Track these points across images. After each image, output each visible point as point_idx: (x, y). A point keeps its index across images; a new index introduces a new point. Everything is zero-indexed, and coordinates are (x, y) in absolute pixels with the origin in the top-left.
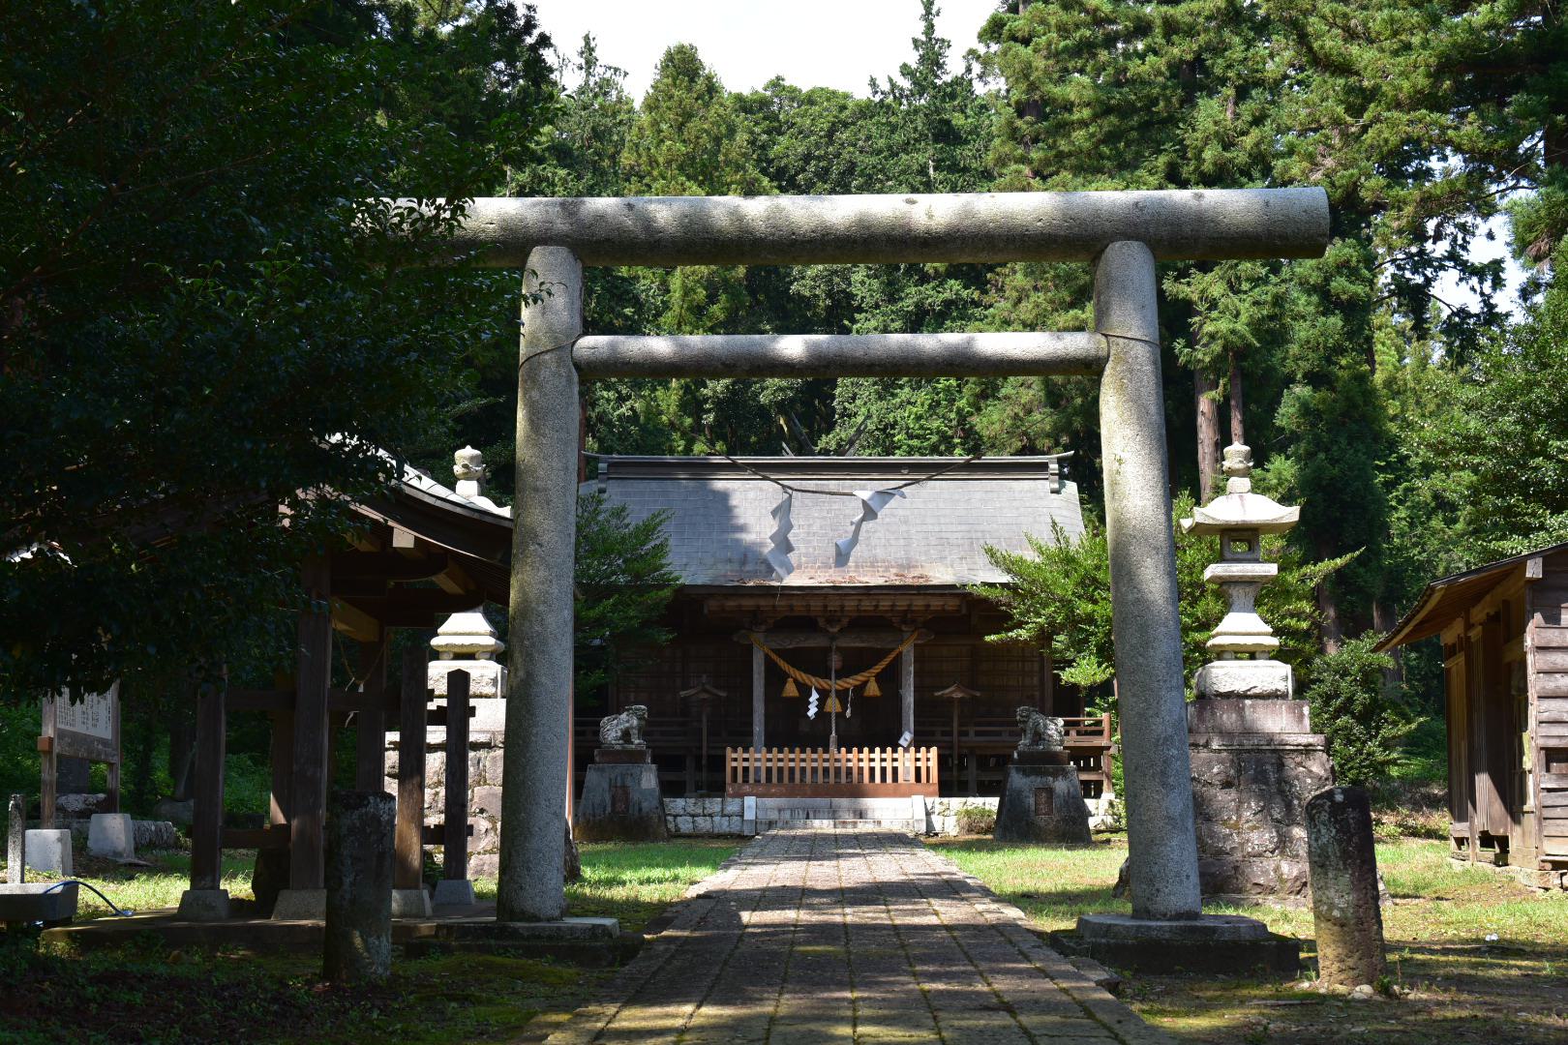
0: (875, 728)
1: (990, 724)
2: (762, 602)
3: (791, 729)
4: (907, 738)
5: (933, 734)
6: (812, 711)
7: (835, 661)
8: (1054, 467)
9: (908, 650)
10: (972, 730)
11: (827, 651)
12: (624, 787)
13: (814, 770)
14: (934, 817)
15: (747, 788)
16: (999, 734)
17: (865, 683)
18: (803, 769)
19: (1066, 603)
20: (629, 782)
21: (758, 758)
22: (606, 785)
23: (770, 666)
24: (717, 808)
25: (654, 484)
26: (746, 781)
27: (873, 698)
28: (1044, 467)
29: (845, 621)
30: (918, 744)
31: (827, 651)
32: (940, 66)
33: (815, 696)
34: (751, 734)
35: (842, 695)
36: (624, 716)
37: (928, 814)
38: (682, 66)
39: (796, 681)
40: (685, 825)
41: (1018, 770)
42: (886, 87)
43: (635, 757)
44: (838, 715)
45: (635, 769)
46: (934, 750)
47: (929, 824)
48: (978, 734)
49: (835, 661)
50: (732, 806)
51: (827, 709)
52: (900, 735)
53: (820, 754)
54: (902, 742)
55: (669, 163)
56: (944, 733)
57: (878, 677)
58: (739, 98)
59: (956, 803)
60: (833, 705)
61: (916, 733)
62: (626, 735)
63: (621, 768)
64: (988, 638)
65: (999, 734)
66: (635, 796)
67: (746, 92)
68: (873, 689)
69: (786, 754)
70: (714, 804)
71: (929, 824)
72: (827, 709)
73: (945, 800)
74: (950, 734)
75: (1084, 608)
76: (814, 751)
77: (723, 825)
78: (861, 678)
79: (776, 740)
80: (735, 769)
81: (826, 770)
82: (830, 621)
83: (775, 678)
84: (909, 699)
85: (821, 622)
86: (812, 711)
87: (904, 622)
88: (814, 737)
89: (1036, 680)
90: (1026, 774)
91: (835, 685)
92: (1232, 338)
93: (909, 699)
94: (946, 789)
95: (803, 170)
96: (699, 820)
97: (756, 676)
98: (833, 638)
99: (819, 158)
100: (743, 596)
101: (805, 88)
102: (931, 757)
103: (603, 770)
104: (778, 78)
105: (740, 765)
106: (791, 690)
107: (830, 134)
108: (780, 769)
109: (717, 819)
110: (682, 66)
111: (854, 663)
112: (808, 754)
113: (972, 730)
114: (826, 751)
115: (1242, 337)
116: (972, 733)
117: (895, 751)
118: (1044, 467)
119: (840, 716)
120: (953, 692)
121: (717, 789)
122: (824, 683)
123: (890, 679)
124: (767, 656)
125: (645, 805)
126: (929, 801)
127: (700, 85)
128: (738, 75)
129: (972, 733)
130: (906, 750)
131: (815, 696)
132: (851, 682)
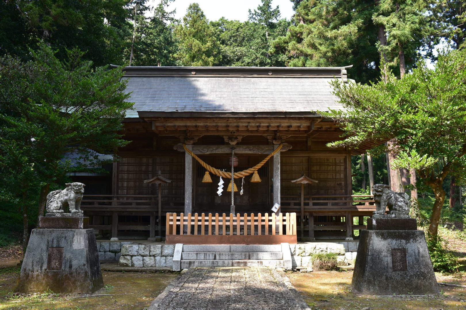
0: (257, 201)
1: (318, 199)
2: (189, 123)
3: (208, 202)
4: (276, 207)
5: (289, 204)
6: (220, 191)
7: (234, 161)
8: (344, 71)
9: (277, 155)
10: (311, 202)
11: (229, 155)
12: (59, 247)
13: (220, 227)
14: (295, 257)
15: (178, 237)
16: (326, 204)
17: (252, 174)
18: (213, 226)
19: (394, 115)
20: (63, 244)
21: (188, 219)
22: (44, 247)
23: (195, 163)
24: (158, 251)
25: (145, 79)
26: (178, 232)
27: (257, 183)
28: (339, 72)
29: (240, 138)
30: (284, 210)
31: (229, 155)
32: (270, 7)
33: (221, 182)
34: (183, 204)
35: (238, 182)
36: (64, 191)
37: (292, 255)
38: (195, 8)
39: (211, 173)
40: (138, 262)
41: (377, 234)
42: (254, 12)
43: (69, 223)
44: (235, 193)
45: (69, 233)
46: (294, 215)
47: (293, 261)
48: (314, 204)
49: (234, 161)
50: (168, 249)
51: (229, 190)
52: (272, 205)
53: (224, 217)
54: (273, 209)
55: (190, 35)
56: (295, 204)
57: (260, 171)
58: (211, 22)
59: (309, 246)
60: (232, 188)
61: (282, 204)
62: (65, 206)
63: (57, 232)
64: (329, 145)
65: (93, 203)
66: (67, 255)
67: (214, 21)
68: (256, 178)
69: (203, 217)
70: (156, 248)
71: (293, 261)
72: (229, 190)
73: (302, 245)
74: (299, 204)
75: (404, 118)
76: (220, 215)
77: (161, 263)
78: (249, 171)
79: (199, 208)
80: (171, 226)
81: (228, 227)
82: (231, 138)
83: (199, 172)
84: (277, 184)
85: (226, 139)
86: (220, 191)
87: (275, 139)
88: (221, 207)
89: (342, 176)
90: (384, 237)
91: (233, 175)
92: (403, 38)
93: (277, 184)
94: (302, 236)
95: (229, 40)
96: (147, 259)
97: (187, 170)
98: (233, 148)
99: (234, 37)
100: (176, 119)
101: (230, 20)
102: (292, 218)
103: (43, 234)
104: (223, 18)
105: (174, 223)
106: (207, 178)
107: (237, 30)
108: (199, 226)
109: (158, 258)
110: (195, 8)
111: (246, 162)
112: (217, 217)
113: (311, 202)
114: (228, 215)
115: (407, 37)
116: (311, 204)
117: (270, 215)
118: (339, 72)
119: (237, 194)
120: (303, 181)
121: (161, 236)
122: (227, 175)
123: (266, 173)
124: (193, 159)
125: (75, 263)
126: (293, 246)
127: (200, 13)
128: (212, 16)
129: (311, 204)
130: (277, 214)
131: (221, 182)
132: (243, 174)
